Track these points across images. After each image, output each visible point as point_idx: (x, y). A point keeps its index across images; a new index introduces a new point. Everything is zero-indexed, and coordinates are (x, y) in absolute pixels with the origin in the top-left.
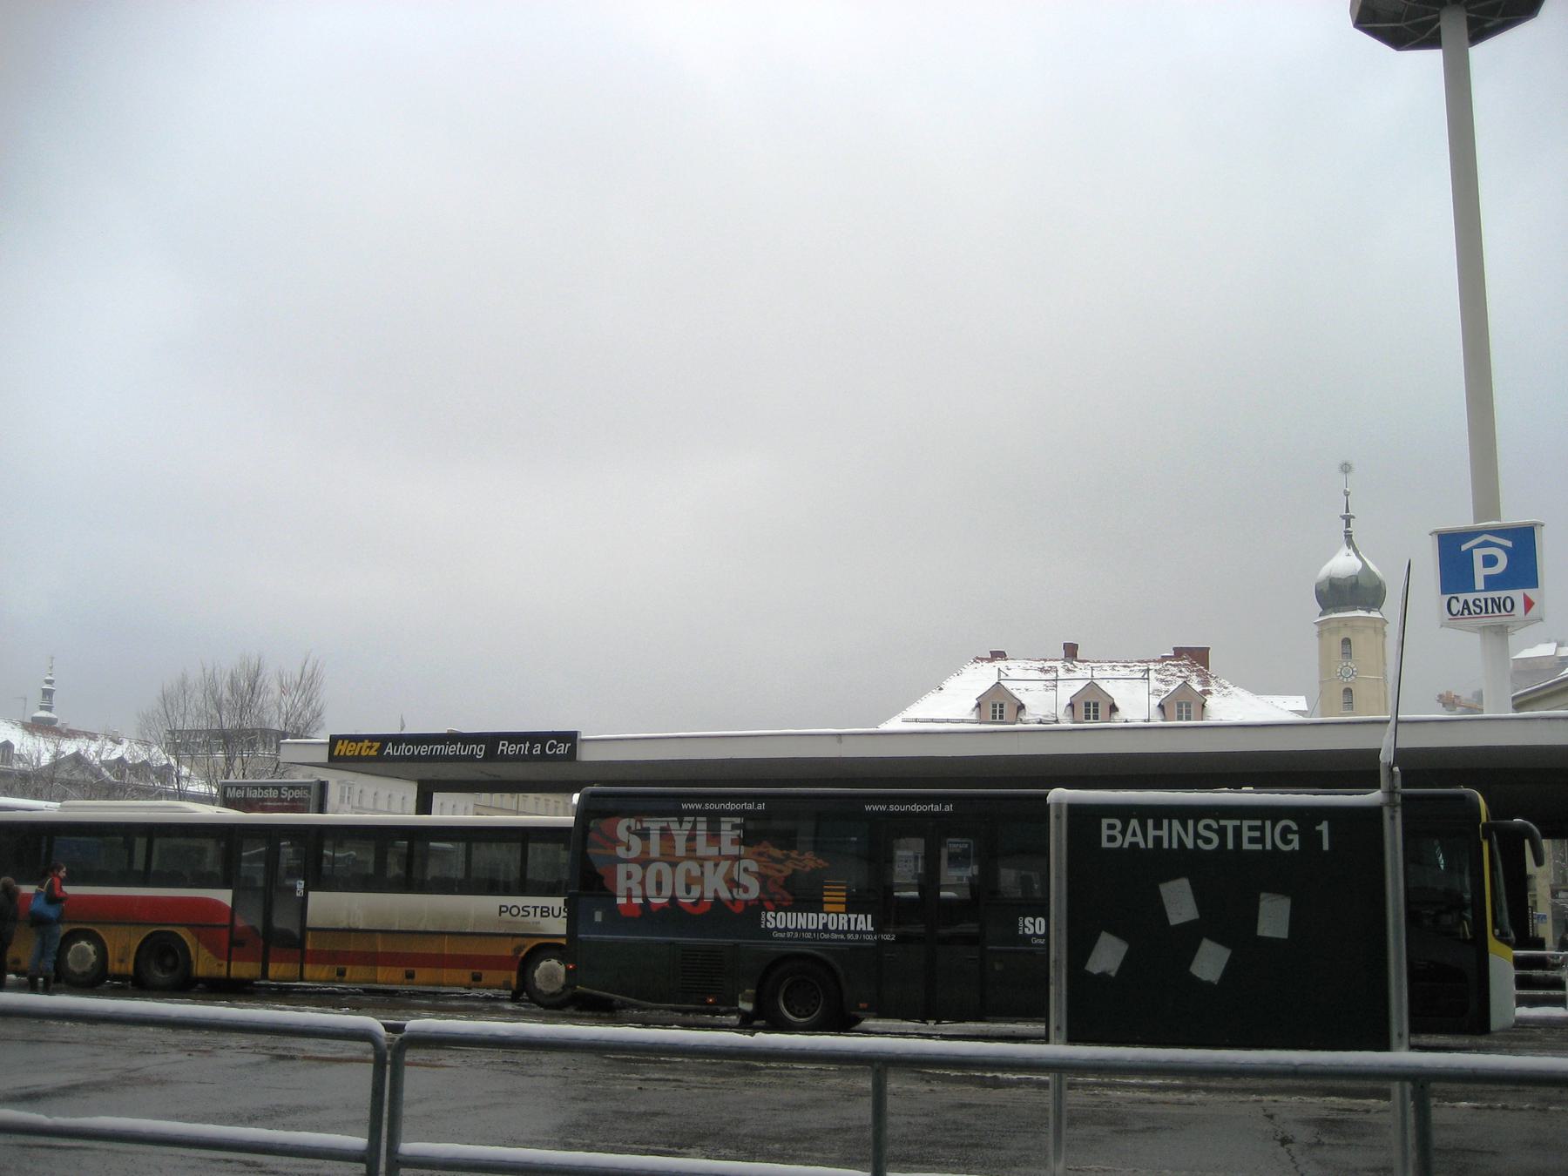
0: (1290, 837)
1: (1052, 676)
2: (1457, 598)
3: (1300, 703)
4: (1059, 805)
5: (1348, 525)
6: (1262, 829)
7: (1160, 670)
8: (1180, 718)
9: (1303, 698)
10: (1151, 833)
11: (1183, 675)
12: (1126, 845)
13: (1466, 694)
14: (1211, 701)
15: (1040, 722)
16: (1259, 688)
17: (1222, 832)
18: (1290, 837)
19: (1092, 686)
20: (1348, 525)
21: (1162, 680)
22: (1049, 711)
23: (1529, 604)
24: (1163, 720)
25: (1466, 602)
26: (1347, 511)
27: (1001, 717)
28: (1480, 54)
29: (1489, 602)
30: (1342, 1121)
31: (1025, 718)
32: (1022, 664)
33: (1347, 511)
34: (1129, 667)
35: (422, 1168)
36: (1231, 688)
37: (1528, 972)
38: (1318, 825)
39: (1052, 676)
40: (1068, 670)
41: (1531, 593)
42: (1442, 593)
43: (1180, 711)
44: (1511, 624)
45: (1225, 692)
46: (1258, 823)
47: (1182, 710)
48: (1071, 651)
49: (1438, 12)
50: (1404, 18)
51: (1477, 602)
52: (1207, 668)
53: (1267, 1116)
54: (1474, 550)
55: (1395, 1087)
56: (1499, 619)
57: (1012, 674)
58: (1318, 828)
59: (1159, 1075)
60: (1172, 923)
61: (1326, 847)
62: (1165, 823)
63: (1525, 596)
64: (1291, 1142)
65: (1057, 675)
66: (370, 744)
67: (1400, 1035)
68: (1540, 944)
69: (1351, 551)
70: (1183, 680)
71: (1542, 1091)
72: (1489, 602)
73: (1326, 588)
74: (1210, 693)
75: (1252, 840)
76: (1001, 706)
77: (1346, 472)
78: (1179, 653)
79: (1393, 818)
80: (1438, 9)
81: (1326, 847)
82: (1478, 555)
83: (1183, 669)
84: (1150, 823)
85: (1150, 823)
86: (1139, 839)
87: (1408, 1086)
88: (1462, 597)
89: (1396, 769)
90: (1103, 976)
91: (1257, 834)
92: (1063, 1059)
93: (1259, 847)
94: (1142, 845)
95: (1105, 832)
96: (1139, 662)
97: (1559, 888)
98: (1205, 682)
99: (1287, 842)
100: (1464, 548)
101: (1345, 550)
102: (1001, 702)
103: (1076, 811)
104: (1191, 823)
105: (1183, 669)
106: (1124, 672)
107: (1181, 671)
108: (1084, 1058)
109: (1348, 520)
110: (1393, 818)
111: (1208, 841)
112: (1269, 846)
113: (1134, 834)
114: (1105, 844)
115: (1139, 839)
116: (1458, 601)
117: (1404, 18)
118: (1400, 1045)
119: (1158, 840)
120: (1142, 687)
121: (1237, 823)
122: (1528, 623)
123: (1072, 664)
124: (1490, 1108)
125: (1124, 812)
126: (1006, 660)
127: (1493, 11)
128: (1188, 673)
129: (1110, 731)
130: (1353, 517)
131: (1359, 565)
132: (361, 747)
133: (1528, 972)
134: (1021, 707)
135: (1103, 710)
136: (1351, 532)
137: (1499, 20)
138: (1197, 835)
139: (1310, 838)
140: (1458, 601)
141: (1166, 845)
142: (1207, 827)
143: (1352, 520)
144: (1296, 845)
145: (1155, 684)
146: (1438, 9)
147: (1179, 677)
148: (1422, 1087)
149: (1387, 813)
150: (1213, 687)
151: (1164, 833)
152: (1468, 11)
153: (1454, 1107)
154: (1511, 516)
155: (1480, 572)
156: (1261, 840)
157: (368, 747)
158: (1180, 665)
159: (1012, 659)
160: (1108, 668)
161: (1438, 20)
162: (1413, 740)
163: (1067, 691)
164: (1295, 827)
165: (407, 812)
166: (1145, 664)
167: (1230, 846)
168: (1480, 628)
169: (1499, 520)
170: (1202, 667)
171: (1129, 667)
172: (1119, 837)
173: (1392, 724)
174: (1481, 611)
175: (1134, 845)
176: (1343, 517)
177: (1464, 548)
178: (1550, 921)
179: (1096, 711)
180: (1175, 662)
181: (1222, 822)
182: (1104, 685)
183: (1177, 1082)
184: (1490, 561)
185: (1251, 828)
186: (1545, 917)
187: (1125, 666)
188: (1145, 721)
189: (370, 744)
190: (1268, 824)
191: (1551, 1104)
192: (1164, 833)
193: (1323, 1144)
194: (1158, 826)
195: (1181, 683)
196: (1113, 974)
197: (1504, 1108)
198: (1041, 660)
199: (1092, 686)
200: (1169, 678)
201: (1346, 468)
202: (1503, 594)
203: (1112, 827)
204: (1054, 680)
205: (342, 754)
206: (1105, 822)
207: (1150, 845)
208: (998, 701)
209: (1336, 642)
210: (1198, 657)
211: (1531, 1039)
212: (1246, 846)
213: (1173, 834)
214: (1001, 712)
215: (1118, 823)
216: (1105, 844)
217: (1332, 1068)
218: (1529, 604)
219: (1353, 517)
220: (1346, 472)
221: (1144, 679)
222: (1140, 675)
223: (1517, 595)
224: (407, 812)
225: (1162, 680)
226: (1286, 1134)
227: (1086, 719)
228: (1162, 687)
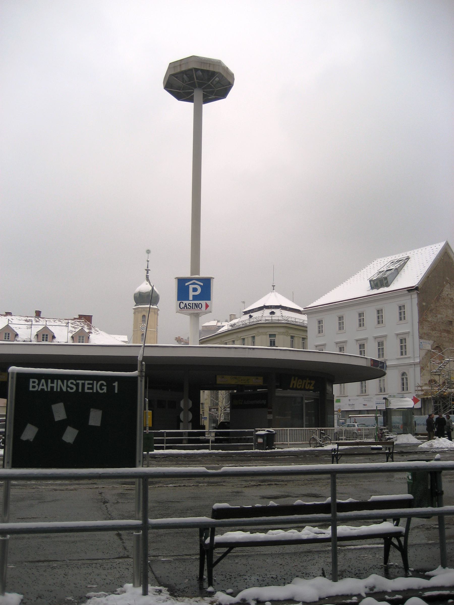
0: (103, 387)
1: (30, 323)
2: (183, 302)
3: (125, 338)
4: (13, 373)
5: (148, 273)
6: (92, 384)
7: (73, 323)
8: (79, 342)
9: (126, 336)
10: (50, 385)
11: (82, 325)
12: (39, 390)
13: (185, 338)
14: (91, 336)
15: (24, 341)
16: (110, 332)
17: (77, 385)
18: (103, 387)
19: (46, 328)
20: (148, 273)
21: (73, 327)
22: (28, 337)
23: (207, 306)
24: (73, 343)
25: (186, 304)
26: (148, 268)
27: (8, 339)
28: (206, 107)
29: (194, 304)
30: (127, 494)
31: (18, 339)
32: (18, 318)
33: (148, 268)
34: (61, 321)
35: (37, 533)
36: (100, 331)
37: (198, 438)
38: (114, 383)
39: (30, 323)
40: (37, 321)
41: (208, 302)
42: (178, 301)
43: (79, 339)
44: (201, 313)
45: (97, 333)
46: (91, 382)
47: (82, 340)
48: (38, 314)
49: (193, 89)
50: (181, 89)
51: (190, 305)
52: (91, 323)
53: (100, 493)
54: (190, 285)
55: (136, 480)
56: (196, 311)
57: (14, 322)
58: (114, 384)
59: (60, 479)
60: (56, 420)
61: (116, 391)
62: (55, 381)
63: (206, 303)
64: (107, 503)
65: (32, 323)
66: (309, 382)
67: (140, 461)
68: (203, 427)
69: (148, 283)
70: (81, 327)
71: (198, 479)
72: (194, 304)
73: (138, 295)
74: (92, 333)
75: (89, 388)
76: (9, 334)
77: (148, 253)
78: (81, 317)
79: (141, 381)
80: (193, 88)
81: (116, 391)
82: (191, 287)
83: (82, 323)
84: (49, 381)
85: (49, 381)
86: (45, 387)
87: (141, 479)
88: (185, 302)
89: (144, 363)
90: (28, 441)
91: (91, 386)
92: (9, 475)
93: (91, 391)
94: (46, 390)
95: (31, 384)
96: (65, 319)
97: (211, 408)
98: (90, 329)
99: (102, 389)
100: (187, 284)
101: (146, 282)
102: (9, 332)
103: (20, 375)
104: (65, 381)
105: (82, 323)
106: (59, 323)
107: (81, 324)
108: (17, 474)
109: (148, 271)
110: (141, 381)
111: (72, 388)
112: (95, 391)
113: (43, 385)
114: (31, 389)
115: (45, 387)
116: (183, 304)
117: (181, 89)
118: (139, 465)
119: (52, 388)
120: (65, 329)
121: (83, 382)
122: (206, 313)
123: (38, 319)
124: (179, 486)
125: (39, 376)
126: (12, 316)
127: (211, 93)
128: (84, 325)
129: (50, 346)
130: (150, 270)
131: (150, 288)
132: (305, 383)
133: (198, 438)
134: (17, 335)
135: (49, 337)
136: (149, 276)
137: (213, 97)
138: (67, 386)
139: (110, 388)
140: (183, 304)
141: (55, 390)
142: (72, 383)
143: (149, 271)
144: (105, 391)
145: (70, 329)
146: (193, 88)
147: (80, 326)
148: (146, 480)
149: (139, 379)
150: (93, 331)
151: (55, 385)
152: (204, 91)
153: (167, 486)
154: (203, 274)
155: (191, 294)
156: (92, 388)
157: (309, 383)
158: (81, 321)
159: (15, 316)
160: (53, 321)
161: (193, 92)
162: (150, 353)
163: (36, 329)
164: (105, 384)
165: (402, 412)
166: (67, 321)
167: (80, 390)
168: (190, 314)
169: (199, 275)
170: (89, 323)
171: (61, 321)
172: (37, 386)
173: (143, 347)
174: (191, 308)
175: (42, 390)
176: (146, 270)
177: (187, 284)
178: (208, 419)
179: (47, 338)
180: (79, 320)
181: (78, 381)
182: (50, 328)
183: (67, 482)
184: (195, 290)
185: (89, 384)
186: (206, 418)
187: (59, 321)
188: (66, 342)
189: (309, 382)
190: (95, 382)
191: (200, 483)
192: (55, 385)
193: (119, 503)
194: (53, 382)
195: (81, 328)
196: (31, 440)
197: (184, 486)
198: (26, 317)
199: (46, 328)
200: (76, 327)
201: (148, 252)
202: (198, 302)
203: (34, 382)
204: (31, 325)
205: (295, 387)
206: (31, 380)
207: (49, 390)
208: (7, 332)
209: (140, 316)
210: (88, 319)
211: (198, 461)
212: (86, 391)
213: (58, 385)
214: (8, 336)
215: (37, 381)
216: (31, 389)
217: (114, 474)
218: (207, 306)
219: (150, 270)
220: (148, 253)
221: (67, 326)
222: (65, 325)
223: (203, 303)
224: (366, 411)
225: (73, 327)
226: (106, 500)
227: (43, 341)
228: (73, 330)
